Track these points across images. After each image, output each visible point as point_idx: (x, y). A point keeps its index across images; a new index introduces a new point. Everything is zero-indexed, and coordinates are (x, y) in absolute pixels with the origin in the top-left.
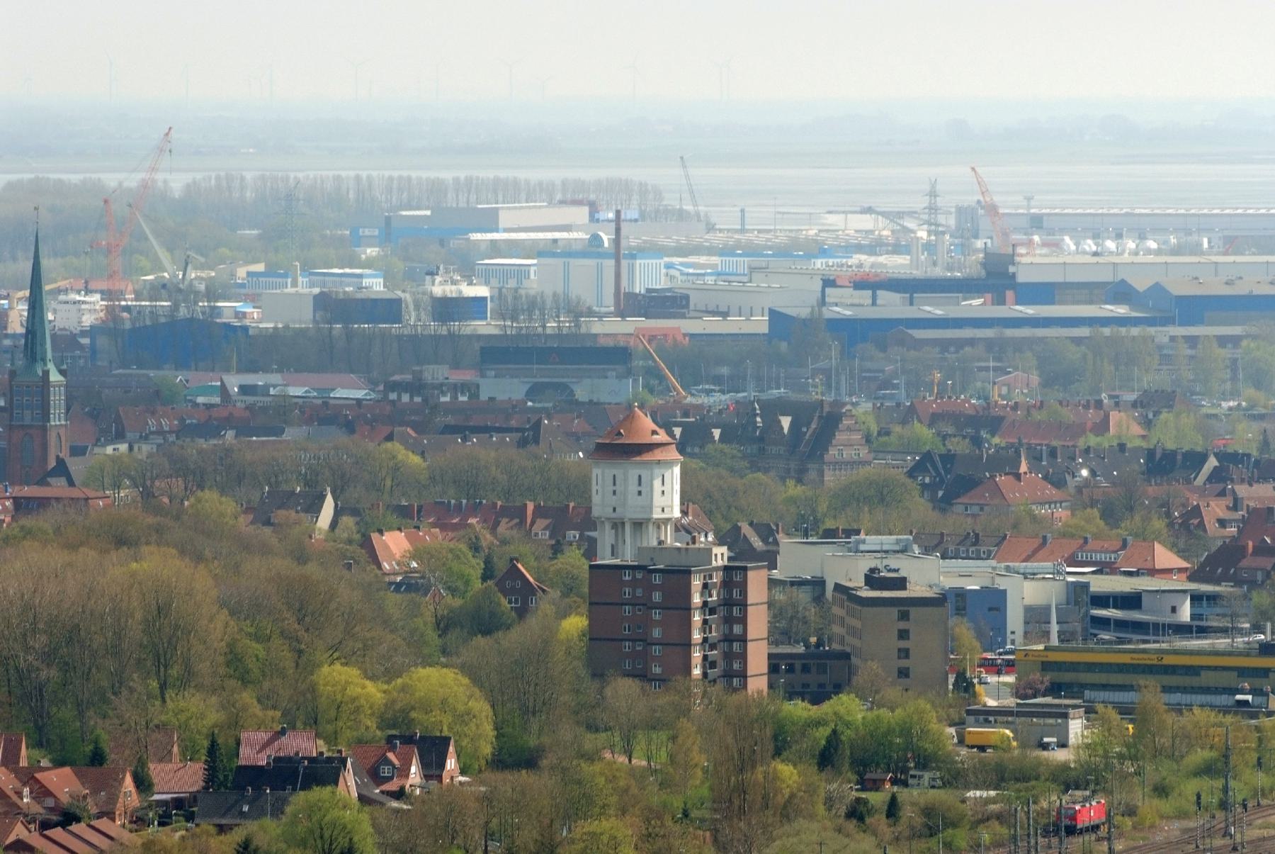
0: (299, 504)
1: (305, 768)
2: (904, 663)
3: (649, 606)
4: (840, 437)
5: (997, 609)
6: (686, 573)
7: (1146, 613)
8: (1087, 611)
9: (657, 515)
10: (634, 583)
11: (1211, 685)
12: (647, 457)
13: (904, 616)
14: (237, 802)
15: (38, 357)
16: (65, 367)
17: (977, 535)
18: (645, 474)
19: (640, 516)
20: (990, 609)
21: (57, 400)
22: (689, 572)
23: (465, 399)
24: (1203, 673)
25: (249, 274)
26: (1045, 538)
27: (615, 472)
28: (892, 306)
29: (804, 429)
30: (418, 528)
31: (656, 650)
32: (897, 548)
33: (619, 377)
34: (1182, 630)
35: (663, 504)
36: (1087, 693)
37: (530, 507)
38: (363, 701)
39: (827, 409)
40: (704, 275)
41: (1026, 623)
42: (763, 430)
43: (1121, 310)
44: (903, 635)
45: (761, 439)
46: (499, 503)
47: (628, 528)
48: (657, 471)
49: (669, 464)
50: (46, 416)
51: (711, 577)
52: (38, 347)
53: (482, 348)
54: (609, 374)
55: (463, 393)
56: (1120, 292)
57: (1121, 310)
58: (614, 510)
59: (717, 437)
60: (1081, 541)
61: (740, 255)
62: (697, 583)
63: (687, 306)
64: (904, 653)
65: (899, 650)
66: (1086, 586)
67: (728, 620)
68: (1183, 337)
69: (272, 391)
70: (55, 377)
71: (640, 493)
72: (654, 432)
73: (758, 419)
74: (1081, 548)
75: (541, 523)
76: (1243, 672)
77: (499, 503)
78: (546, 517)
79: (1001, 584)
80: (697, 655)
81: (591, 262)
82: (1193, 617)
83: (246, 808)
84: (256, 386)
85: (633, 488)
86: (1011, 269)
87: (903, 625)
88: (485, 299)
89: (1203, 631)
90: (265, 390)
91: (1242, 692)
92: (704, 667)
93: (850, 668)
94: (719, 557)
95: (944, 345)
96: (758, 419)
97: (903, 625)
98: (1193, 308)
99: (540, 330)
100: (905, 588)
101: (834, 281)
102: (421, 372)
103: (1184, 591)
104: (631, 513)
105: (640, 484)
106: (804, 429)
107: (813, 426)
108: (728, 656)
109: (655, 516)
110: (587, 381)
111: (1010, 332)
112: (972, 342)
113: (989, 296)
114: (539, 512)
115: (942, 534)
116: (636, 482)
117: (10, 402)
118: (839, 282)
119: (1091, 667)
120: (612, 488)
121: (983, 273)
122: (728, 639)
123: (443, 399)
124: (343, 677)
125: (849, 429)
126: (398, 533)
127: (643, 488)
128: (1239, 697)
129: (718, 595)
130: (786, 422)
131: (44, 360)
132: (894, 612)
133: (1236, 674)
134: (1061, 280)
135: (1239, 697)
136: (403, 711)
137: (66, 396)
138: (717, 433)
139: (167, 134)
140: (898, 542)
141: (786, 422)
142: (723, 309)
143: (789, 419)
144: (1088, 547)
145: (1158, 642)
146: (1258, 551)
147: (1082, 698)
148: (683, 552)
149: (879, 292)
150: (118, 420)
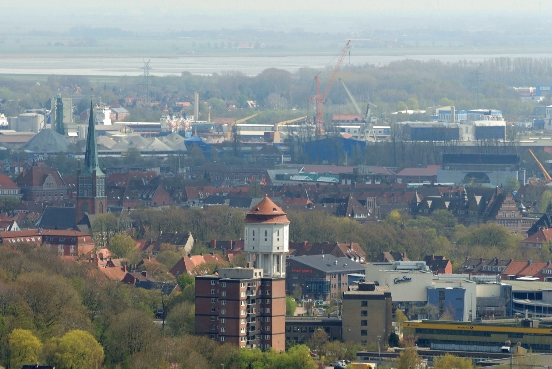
0: (176, 240)
2: (364, 328)
3: (218, 298)
4: (504, 206)
5: (460, 299)
6: (235, 283)
7: (545, 302)
9: (275, 251)
11: (495, 341)
12: (269, 222)
13: (365, 304)
15: (91, 164)
16: (105, 169)
17: (497, 260)
18: (269, 230)
20: (457, 299)
21: (100, 186)
22: (239, 282)
24: (492, 335)
25: (440, 112)
26: (529, 262)
29: (487, 202)
30: (212, 254)
32: (416, 268)
33: (512, 170)
36: (432, 344)
38: (29, 348)
39: (499, 193)
41: (477, 306)
42: (468, 203)
45: (467, 207)
48: (275, 229)
49: (282, 225)
50: (94, 194)
51: (253, 284)
52: (91, 159)
53: (444, 155)
54: (506, 168)
55: (378, 180)
58: (254, 248)
59: (447, 206)
60: (546, 264)
62: (243, 287)
64: (365, 323)
65: (362, 321)
66: (510, 288)
69: (291, 178)
70: (99, 173)
71: (266, 240)
72: (274, 209)
73: (466, 197)
74: (545, 267)
76: (510, 335)
79: (465, 286)
80: (243, 323)
84: (283, 175)
85: (263, 237)
87: (364, 308)
88: (503, 127)
90: (287, 178)
91: (507, 345)
93: (341, 329)
94: (258, 274)
96: (466, 197)
97: (364, 308)
99: (495, 145)
102: (357, 169)
105: (266, 235)
106: (487, 202)
107: (492, 201)
108: (263, 324)
109: (274, 251)
110: (495, 172)
115: (481, 259)
117: (78, 185)
119: (440, 331)
120: (252, 237)
123: (367, 183)
124: (21, 335)
125: (509, 202)
126: (200, 256)
127: (268, 237)
128: (504, 348)
129: (257, 293)
130: (478, 199)
131: (94, 165)
132: (360, 302)
133: (507, 335)
135: (504, 348)
137: (106, 185)
139: (348, 44)
140: (417, 264)
141: (478, 199)
144: (549, 266)
145: (545, 316)
147: (430, 347)
150: (185, 193)
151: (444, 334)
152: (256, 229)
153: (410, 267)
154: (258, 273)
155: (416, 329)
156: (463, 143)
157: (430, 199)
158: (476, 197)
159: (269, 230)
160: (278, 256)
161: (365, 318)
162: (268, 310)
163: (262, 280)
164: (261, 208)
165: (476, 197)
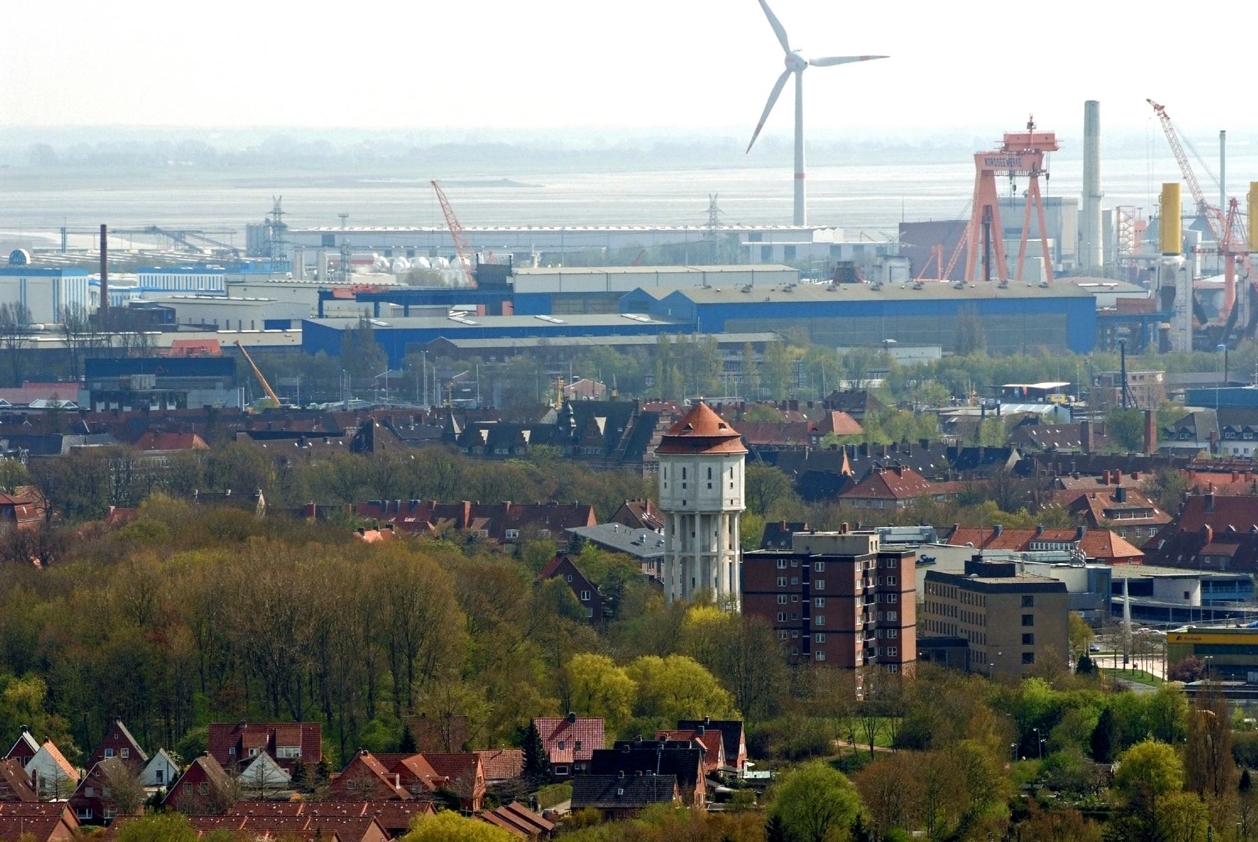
1: (663, 752)
6: (851, 561)
8: (1108, 600)
10: (789, 572)
12: (717, 450)
13: (1028, 602)
14: (611, 785)
19: (708, 508)
23: (173, 408)
26: (996, 529)
27: (686, 465)
28: (387, 318)
29: (620, 430)
31: (820, 638)
32: (920, 538)
34: (1195, 614)
35: (684, 497)
37: (468, 505)
40: (128, 291)
43: (644, 319)
44: (1027, 620)
45: (575, 440)
46: (435, 503)
47: (698, 520)
48: (726, 464)
49: (735, 456)
56: (638, 300)
57: (644, 319)
58: (684, 503)
60: (1034, 532)
61: (159, 271)
62: (858, 569)
63: (173, 320)
64: (1027, 639)
67: (882, 608)
68: (754, 344)
71: (710, 486)
72: (721, 426)
73: (572, 420)
75: (480, 522)
77: (435, 503)
78: (483, 516)
81: (14, 279)
82: (1204, 601)
83: (621, 792)
85: (703, 481)
86: (509, 280)
89: (1220, 616)
92: (864, 654)
95: (485, 353)
96: (572, 420)
97: (1026, 611)
98: (716, 316)
100: (1013, 574)
101: (331, 293)
102: (129, 381)
103: (1196, 577)
104: (704, 506)
105: (710, 477)
109: (725, 508)
111: (554, 341)
112: (511, 351)
113: (483, 306)
114: (476, 511)
116: (706, 475)
118: (337, 295)
120: (681, 481)
121: (474, 285)
122: (883, 626)
123: (153, 408)
124: (597, 666)
130: (601, 422)
132: (1018, 598)
134: (557, 290)
136: (653, 698)
138: (527, 434)
141: (601, 422)
142: (209, 322)
143: (604, 419)
146: (1218, 538)
147: (1245, 680)
148: (839, 541)
149: (382, 304)
151: (1242, 653)
152: (688, 465)
153: (910, 538)
154: (875, 544)
155: (1195, 645)
156: (1241, 297)
157: (484, 427)
158: (597, 419)
159: (715, 466)
160: (732, 514)
161: (1028, 630)
162: (892, 616)
163: (880, 557)
164: (697, 424)
165: (597, 419)
